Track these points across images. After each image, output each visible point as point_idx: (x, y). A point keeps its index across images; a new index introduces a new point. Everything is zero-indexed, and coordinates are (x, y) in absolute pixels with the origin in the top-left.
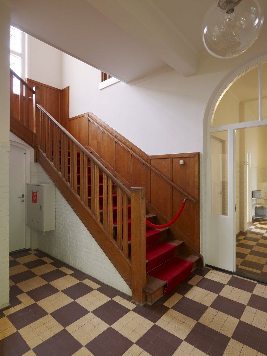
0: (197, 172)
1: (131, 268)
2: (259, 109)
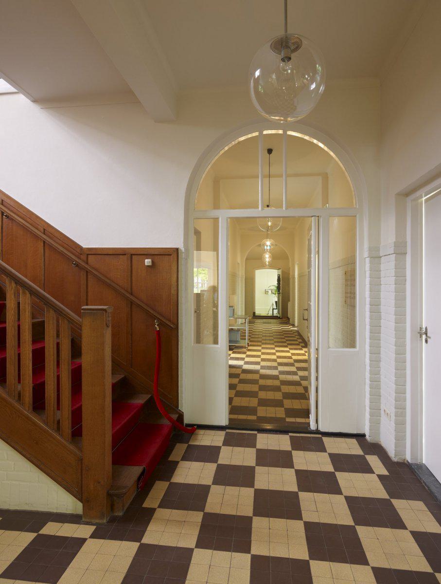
0: (174, 279)
1: (81, 460)
2: (260, 194)
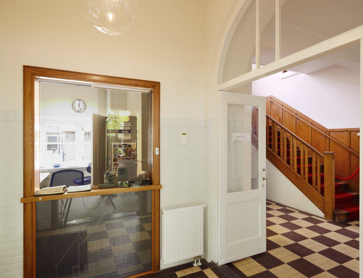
1: (323, 200)
